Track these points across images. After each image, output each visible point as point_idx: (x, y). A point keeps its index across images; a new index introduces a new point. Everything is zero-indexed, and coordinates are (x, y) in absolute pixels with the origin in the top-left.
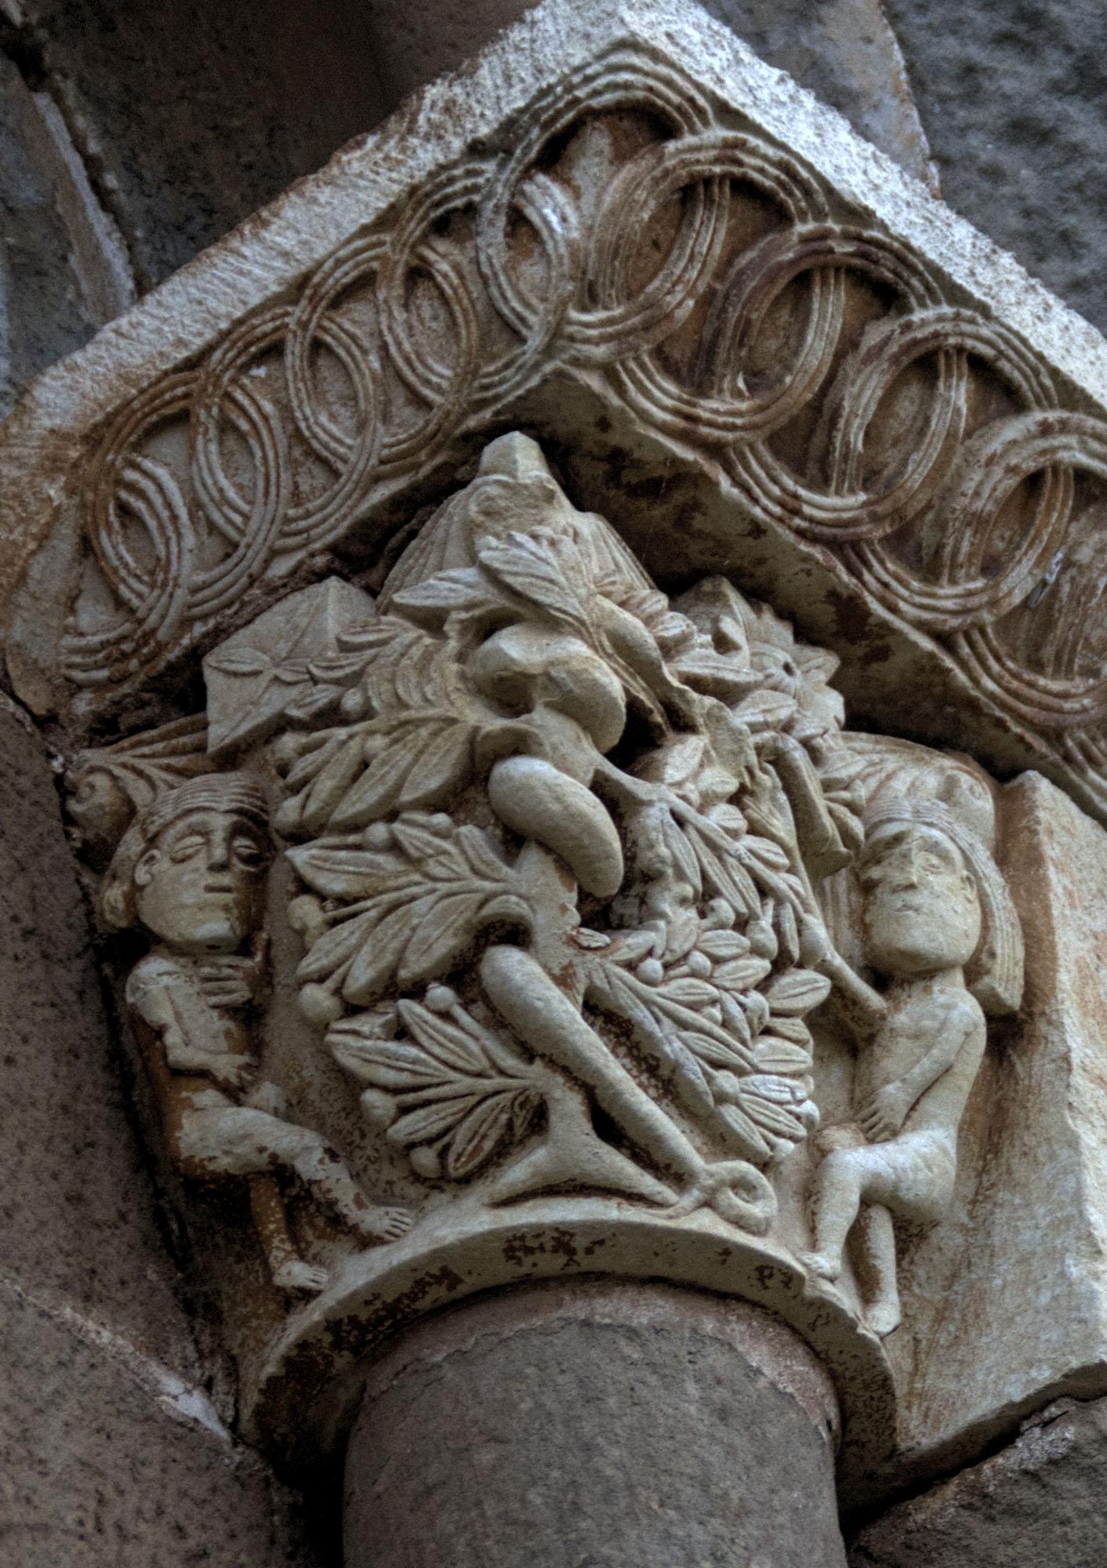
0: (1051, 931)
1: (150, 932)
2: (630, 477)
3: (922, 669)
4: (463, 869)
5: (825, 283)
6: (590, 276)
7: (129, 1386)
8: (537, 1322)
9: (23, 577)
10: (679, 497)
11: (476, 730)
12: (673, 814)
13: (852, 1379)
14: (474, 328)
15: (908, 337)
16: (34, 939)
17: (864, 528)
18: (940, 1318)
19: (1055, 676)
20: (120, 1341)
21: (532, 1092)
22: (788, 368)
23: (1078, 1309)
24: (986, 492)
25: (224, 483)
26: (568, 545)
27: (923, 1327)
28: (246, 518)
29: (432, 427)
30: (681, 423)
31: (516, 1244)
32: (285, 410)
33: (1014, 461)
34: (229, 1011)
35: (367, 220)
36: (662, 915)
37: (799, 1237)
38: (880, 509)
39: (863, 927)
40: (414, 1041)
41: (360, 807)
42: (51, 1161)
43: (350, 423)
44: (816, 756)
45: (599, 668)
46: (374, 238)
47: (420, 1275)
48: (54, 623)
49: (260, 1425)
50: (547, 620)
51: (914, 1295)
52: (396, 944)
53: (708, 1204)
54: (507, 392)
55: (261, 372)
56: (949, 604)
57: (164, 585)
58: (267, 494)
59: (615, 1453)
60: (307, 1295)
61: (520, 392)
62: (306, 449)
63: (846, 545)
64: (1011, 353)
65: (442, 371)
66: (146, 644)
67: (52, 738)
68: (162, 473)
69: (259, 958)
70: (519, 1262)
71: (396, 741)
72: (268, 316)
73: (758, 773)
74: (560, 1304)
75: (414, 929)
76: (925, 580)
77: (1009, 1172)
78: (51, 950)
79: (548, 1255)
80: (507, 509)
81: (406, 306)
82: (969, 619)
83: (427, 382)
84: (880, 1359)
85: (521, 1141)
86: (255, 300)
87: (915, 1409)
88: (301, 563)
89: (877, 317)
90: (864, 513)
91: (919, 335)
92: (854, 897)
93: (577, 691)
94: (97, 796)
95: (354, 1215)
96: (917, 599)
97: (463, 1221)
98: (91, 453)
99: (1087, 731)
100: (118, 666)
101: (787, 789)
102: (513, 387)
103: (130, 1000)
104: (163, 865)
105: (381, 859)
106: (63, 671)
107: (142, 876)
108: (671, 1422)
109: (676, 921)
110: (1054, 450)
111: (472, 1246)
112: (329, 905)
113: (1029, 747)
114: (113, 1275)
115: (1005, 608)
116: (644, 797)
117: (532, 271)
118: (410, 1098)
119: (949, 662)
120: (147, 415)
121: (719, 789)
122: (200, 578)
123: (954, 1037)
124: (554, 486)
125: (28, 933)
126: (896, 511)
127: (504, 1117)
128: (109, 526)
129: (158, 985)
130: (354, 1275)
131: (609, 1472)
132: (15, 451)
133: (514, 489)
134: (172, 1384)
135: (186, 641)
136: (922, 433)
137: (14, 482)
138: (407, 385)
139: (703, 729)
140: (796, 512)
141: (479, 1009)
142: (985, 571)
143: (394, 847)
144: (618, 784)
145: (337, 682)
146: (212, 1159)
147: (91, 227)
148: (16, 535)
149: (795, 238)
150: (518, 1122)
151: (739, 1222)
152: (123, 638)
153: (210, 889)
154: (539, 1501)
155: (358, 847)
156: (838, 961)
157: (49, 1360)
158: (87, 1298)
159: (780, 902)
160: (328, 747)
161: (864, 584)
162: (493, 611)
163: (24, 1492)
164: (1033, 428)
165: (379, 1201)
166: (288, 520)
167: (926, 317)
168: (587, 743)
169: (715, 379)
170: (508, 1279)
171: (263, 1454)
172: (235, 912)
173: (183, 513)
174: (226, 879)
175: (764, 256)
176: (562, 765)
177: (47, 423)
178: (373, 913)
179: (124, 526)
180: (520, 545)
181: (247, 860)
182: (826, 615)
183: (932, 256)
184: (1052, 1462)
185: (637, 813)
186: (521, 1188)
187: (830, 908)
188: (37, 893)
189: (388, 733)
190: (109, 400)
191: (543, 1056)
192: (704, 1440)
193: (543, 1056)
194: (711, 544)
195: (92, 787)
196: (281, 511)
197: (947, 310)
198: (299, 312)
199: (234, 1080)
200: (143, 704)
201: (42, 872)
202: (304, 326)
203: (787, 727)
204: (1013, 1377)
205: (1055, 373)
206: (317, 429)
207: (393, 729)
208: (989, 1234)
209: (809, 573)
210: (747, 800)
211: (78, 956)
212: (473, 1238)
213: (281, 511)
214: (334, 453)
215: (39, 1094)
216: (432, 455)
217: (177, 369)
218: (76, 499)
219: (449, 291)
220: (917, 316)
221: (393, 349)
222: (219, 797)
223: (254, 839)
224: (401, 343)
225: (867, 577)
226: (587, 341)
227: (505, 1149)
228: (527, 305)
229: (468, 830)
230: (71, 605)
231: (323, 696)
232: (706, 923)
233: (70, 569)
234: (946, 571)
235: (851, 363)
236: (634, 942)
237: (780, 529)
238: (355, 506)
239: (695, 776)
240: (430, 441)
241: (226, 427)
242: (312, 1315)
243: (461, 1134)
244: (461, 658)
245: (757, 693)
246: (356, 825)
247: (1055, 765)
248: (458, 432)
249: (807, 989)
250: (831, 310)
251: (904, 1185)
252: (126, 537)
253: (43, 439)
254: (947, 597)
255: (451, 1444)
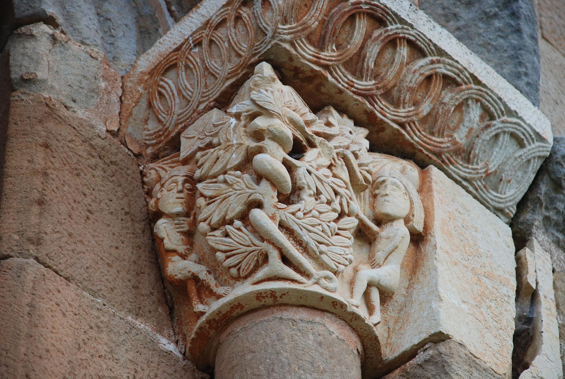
0: (433, 209)
1: (161, 211)
2: (301, 76)
3: (395, 134)
4: (244, 187)
5: (360, 18)
6: (285, 15)
7: (149, 340)
8: (266, 318)
9: (131, 114)
10: (316, 82)
11: (248, 146)
12: (307, 170)
13: (365, 337)
14: (253, 33)
15: (387, 34)
16: (129, 216)
17: (374, 92)
18: (396, 322)
19: (438, 136)
20: (147, 328)
21: (263, 251)
22: (349, 43)
23: (434, 316)
24: (414, 81)
25: (187, 83)
26: (276, 93)
27: (391, 324)
28: (192, 93)
29: (242, 62)
30: (315, 59)
31: (259, 295)
32: (203, 61)
33: (422, 72)
34: (183, 233)
35: (224, 3)
36: (304, 199)
37: (348, 294)
38: (379, 85)
39: (373, 207)
40: (230, 237)
41: (216, 170)
42: (129, 276)
43: (220, 63)
44: (356, 156)
45: (284, 127)
46: (226, 8)
47: (232, 305)
48: (141, 127)
49: (191, 353)
50: (269, 114)
51: (388, 315)
52: (225, 209)
53: (317, 283)
54: (262, 51)
55: (196, 50)
56: (403, 115)
57: (170, 115)
58: (198, 86)
59: (286, 354)
60: (202, 313)
61: (266, 50)
62: (209, 72)
63: (369, 96)
64: (420, 39)
65: (245, 46)
66: (166, 132)
67: (140, 160)
68: (170, 82)
69: (192, 218)
70: (261, 301)
71: (227, 151)
72: (198, 34)
73: (336, 160)
74: (273, 313)
75: (230, 205)
76: (395, 107)
77: (418, 279)
78: (135, 219)
79: (269, 299)
80: (261, 84)
81: (235, 28)
82: (409, 119)
83: (241, 49)
84: (374, 331)
85: (261, 266)
86: (194, 29)
87: (388, 348)
88: (207, 105)
89: (377, 28)
90: (374, 87)
91: (390, 33)
92: (371, 199)
93: (277, 134)
94: (152, 175)
95: (215, 289)
96: (392, 113)
97: (245, 289)
98: (151, 78)
99: (449, 154)
100: (159, 139)
101: (347, 165)
102: (264, 49)
103: (155, 231)
104: (165, 192)
105: (222, 185)
106: (144, 141)
107: (159, 196)
108: (304, 346)
109: (307, 201)
110: (435, 68)
111: (246, 296)
112: (207, 199)
113: (430, 158)
114: (147, 309)
115: (421, 116)
116: (298, 165)
117: (269, 14)
118: (229, 254)
119: (403, 132)
120: (166, 65)
121: (323, 164)
122: (180, 112)
123: (398, 238)
124: (276, 77)
125: (127, 213)
126: (384, 86)
127: (256, 258)
128: (156, 98)
129: (163, 227)
130: (213, 307)
131: (283, 360)
132: (131, 79)
133: (263, 78)
134: (164, 341)
135: (176, 130)
136: (392, 63)
137: (131, 88)
138: (235, 51)
139: (318, 147)
140: (352, 86)
141: (249, 228)
142: (414, 105)
143: (225, 182)
144: (290, 161)
145: (211, 136)
146: (176, 275)
147: (167, 22)
148: (130, 102)
149: (350, 4)
150: (260, 260)
151: (326, 289)
152: (160, 131)
153: (177, 198)
154: (263, 369)
155: (216, 182)
156: (362, 216)
157: (122, 331)
158: (137, 315)
159: (341, 197)
160: (208, 155)
161: (375, 108)
162: (254, 112)
163: (110, 367)
164: (428, 62)
165: (222, 285)
166: (203, 93)
167: (392, 28)
168: (281, 150)
169: (326, 47)
170: (258, 306)
171: (192, 362)
172: (184, 204)
173: (176, 93)
174: (182, 195)
175: (340, 10)
176: (272, 155)
177: (140, 70)
178: (219, 201)
179: (160, 98)
180: (261, 93)
181: (188, 190)
182: (364, 118)
183: (394, 9)
184: (425, 361)
185: (296, 170)
186: (260, 279)
187: (362, 202)
188: (131, 203)
189: (225, 149)
190: (156, 62)
191: (266, 240)
192: (313, 351)
193: (266, 240)
194: (327, 96)
195: (150, 173)
196: (202, 90)
197: (399, 26)
198: (206, 32)
199: (184, 253)
200: (165, 150)
201: (133, 197)
202: (207, 36)
203: (347, 148)
204: (415, 337)
205: (435, 45)
206: (211, 66)
207: (226, 148)
208: (411, 297)
209: (357, 105)
210: (333, 168)
211: (143, 221)
212: (247, 294)
213: (202, 90)
214: (215, 72)
215: (127, 258)
216: (242, 71)
217: (174, 51)
218: (147, 91)
219: (246, 22)
220: (390, 28)
221: (231, 40)
222: (181, 172)
223: (191, 184)
224: (234, 39)
225: (376, 106)
226: (284, 34)
227: (257, 267)
228: (267, 24)
229: (246, 176)
230: (146, 121)
231: (208, 140)
232: (318, 202)
233: (145, 111)
234: (402, 105)
235: (369, 42)
236: (293, 208)
237: (347, 91)
238: (222, 87)
239: (315, 160)
240: (242, 67)
241: (187, 67)
242: (203, 319)
243: (243, 265)
244: (245, 126)
245: (337, 138)
246: (215, 176)
247: (439, 163)
248: (249, 63)
249: (351, 223)
250: (362, 26)
251: (381, 281)
252: (161, 101)
253: (138, 75)
254: (402, 112)
255: (240, 354)
